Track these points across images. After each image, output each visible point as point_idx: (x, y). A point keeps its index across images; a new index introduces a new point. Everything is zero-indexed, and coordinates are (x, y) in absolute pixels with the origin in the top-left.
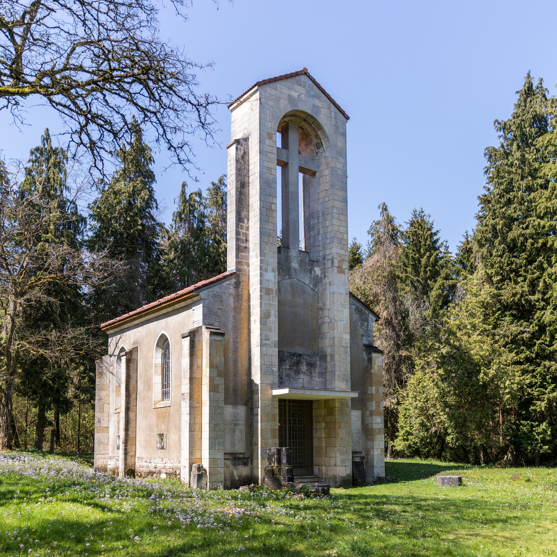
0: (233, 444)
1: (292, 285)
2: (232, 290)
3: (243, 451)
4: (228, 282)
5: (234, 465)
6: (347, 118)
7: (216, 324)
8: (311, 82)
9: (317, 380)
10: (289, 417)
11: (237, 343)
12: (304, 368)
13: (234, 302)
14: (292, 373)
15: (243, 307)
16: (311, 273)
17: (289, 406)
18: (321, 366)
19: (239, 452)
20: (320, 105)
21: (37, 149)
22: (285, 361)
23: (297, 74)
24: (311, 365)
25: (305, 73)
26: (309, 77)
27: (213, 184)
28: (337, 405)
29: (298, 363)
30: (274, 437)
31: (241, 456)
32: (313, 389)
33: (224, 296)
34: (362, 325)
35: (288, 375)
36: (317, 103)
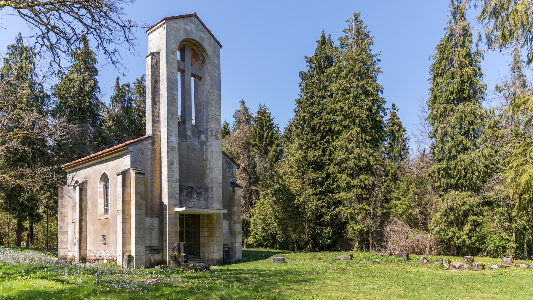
0: (151, 241)
1: (187, 145)
2: (150, 147)
3: (157, 245)
4: (147, 142)
5: (152, 254)
6: (221, 46)
7: (140, 167)
8: (198, 22)
9: (203, 202)
10: (186, 224)
11: (153, 179)
12: (195, 195)
13: (151, 154)
14: (187, 198)
15: (157, 158)
16: (199, 138)
17: (186, 218)
18: (205, 194)
19: (154, 245)
20: (204, 37)
21: (13, 46)
22: (183, 191)
23: (190, 16)
24: (199, 194)
25: (195, 15)
26: (197, 18)
27: (138, 80)
28: (214, 217)
29: (191, 192)
30: (176, 236)
31: (156, 248)
32: (200, 208)
33: (145, 150)
34: (229, 171)
35: (185, 199)
36: (203, 35)
